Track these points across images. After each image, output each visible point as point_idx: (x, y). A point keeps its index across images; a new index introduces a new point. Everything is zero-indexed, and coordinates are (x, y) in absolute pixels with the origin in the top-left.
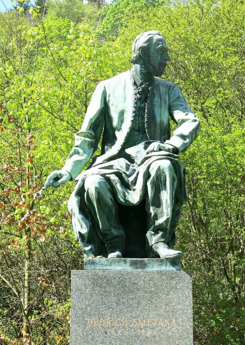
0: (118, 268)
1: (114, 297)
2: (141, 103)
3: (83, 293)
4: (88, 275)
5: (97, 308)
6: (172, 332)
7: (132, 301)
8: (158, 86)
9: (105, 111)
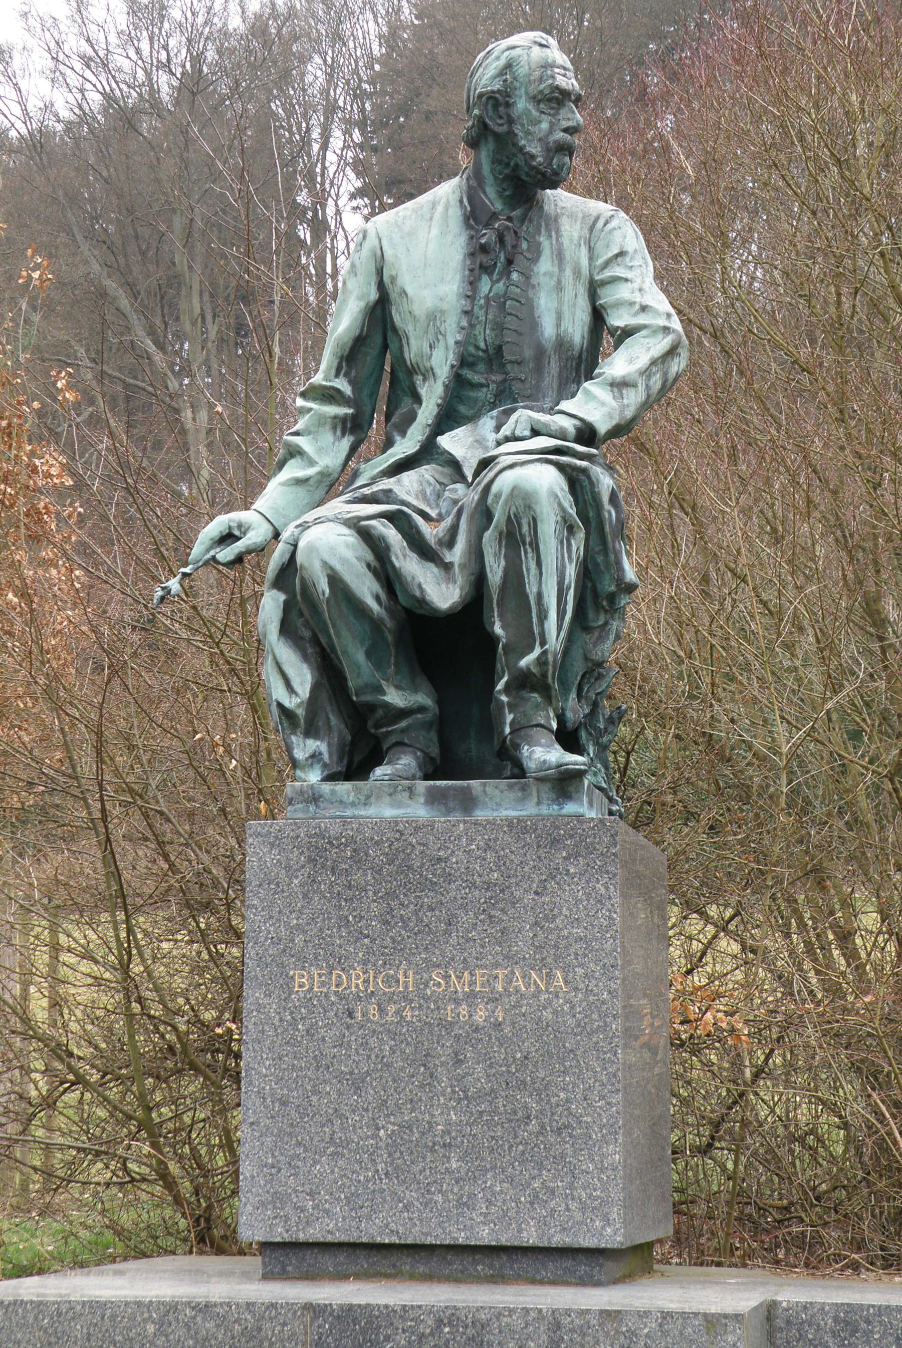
0: (389, 812)
1: (375, 901)
2: (494, 283)
3: (283, 891)
4: (298, 837)
5: (323, 939)
6: (555, 1012)
7: (429, 914)
8: (556, 219)
9: (380, 316)
